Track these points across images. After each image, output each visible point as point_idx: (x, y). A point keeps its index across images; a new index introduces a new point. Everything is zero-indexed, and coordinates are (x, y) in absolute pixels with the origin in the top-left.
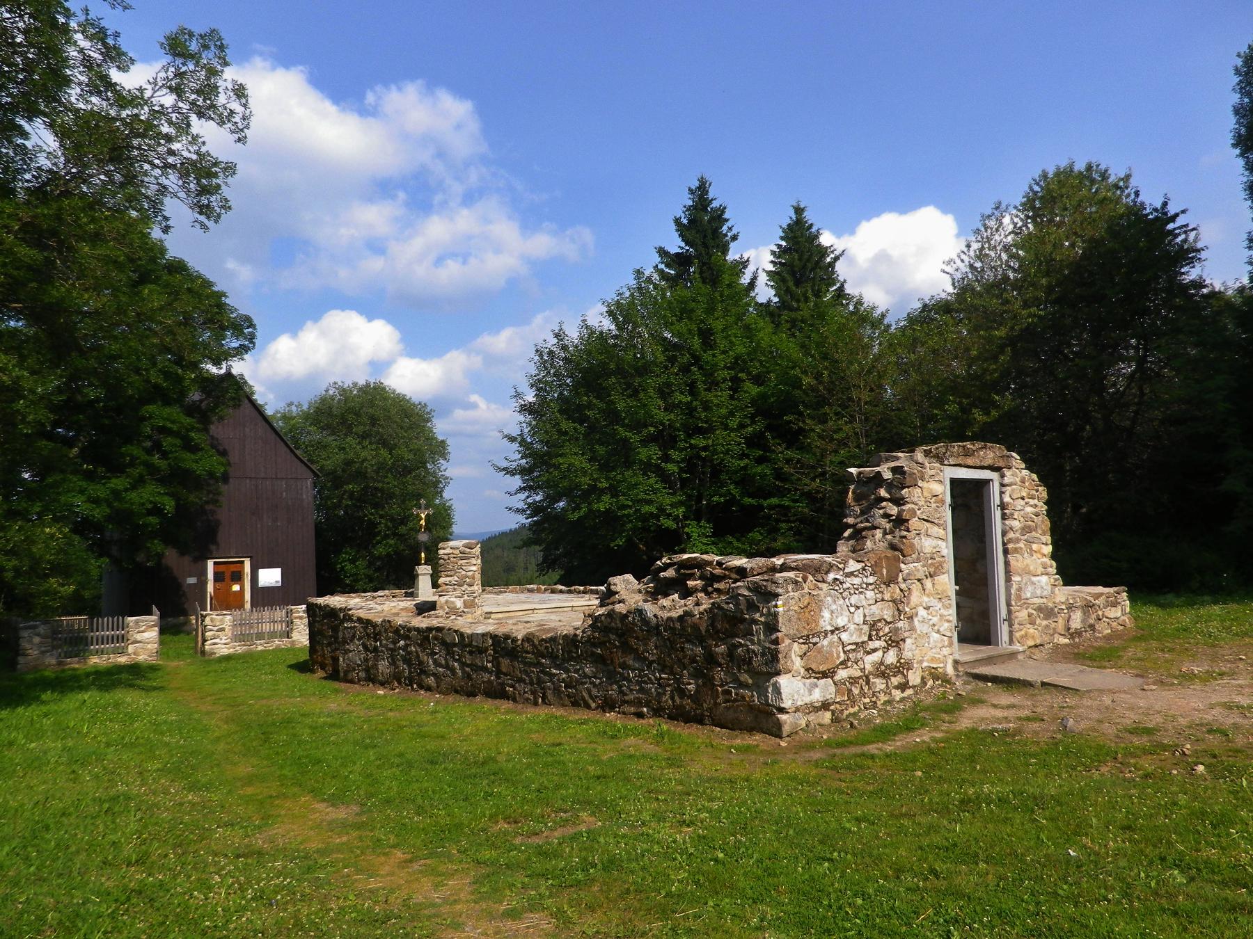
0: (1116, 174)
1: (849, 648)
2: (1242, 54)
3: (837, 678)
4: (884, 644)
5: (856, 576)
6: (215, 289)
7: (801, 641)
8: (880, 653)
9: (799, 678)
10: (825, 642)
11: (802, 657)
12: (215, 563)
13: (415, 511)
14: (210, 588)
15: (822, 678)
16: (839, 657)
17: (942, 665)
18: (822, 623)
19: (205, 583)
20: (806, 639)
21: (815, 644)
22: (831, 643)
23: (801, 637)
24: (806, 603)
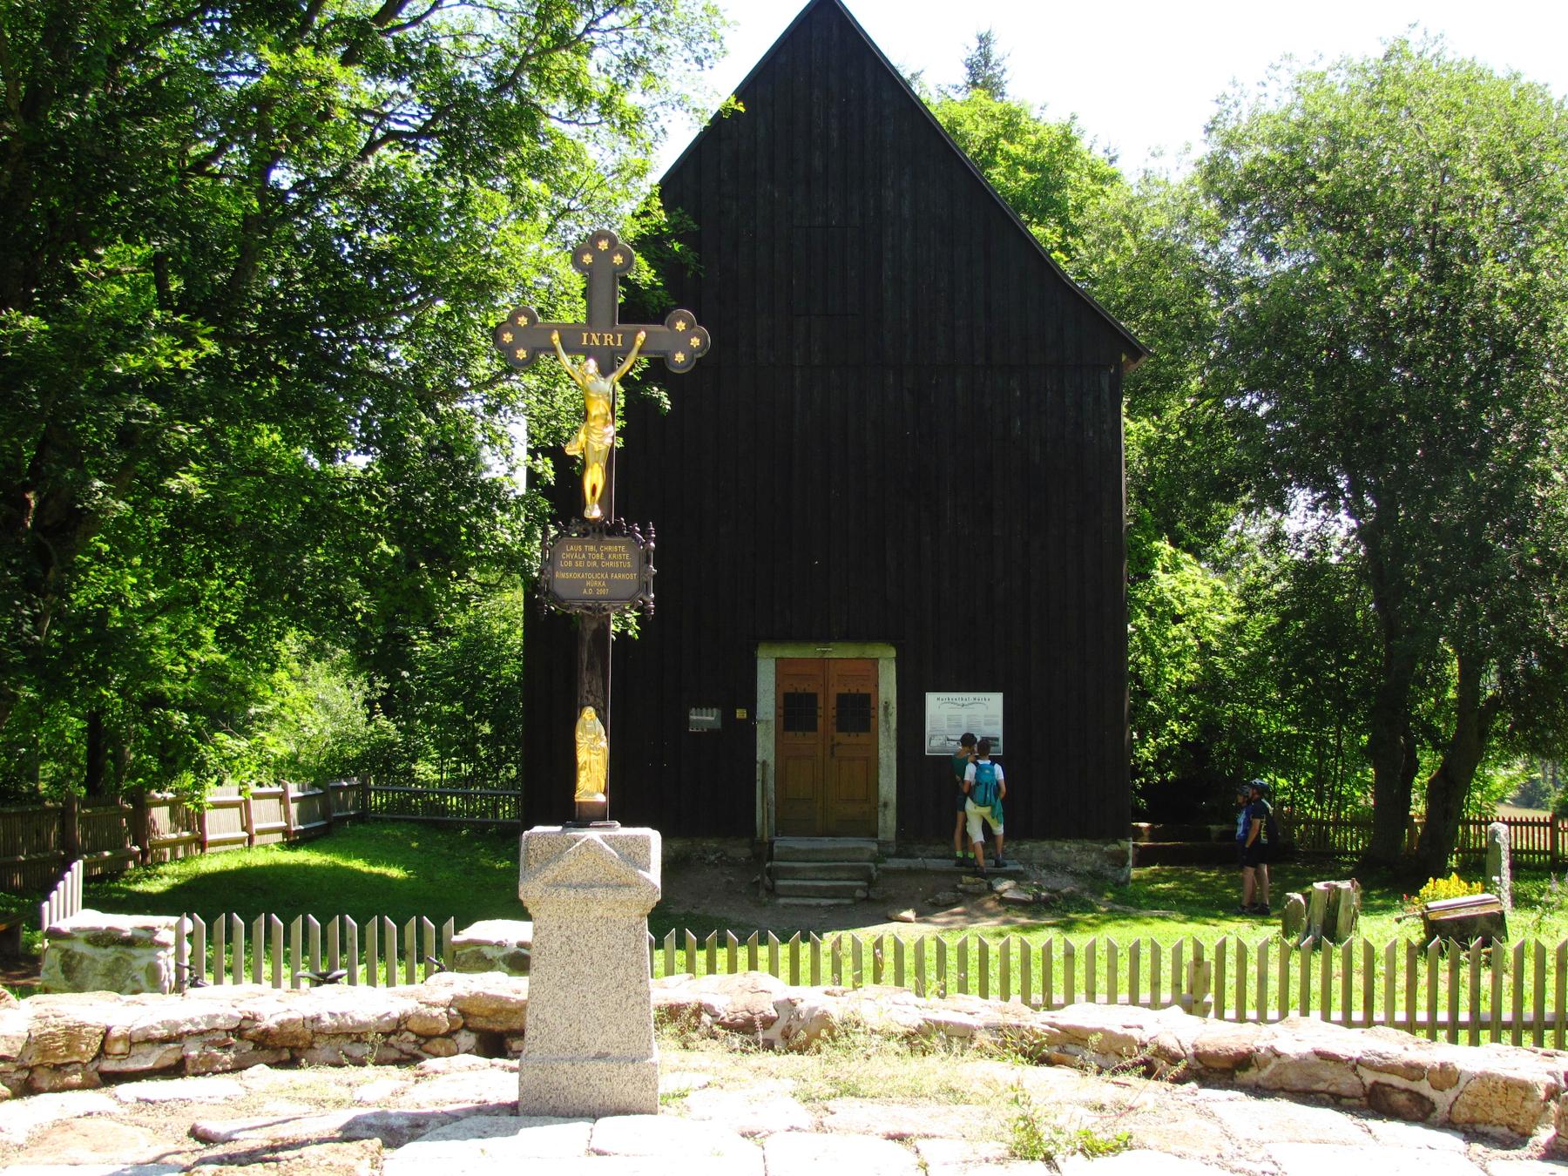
12: (780, 661)
14: (765, 747)
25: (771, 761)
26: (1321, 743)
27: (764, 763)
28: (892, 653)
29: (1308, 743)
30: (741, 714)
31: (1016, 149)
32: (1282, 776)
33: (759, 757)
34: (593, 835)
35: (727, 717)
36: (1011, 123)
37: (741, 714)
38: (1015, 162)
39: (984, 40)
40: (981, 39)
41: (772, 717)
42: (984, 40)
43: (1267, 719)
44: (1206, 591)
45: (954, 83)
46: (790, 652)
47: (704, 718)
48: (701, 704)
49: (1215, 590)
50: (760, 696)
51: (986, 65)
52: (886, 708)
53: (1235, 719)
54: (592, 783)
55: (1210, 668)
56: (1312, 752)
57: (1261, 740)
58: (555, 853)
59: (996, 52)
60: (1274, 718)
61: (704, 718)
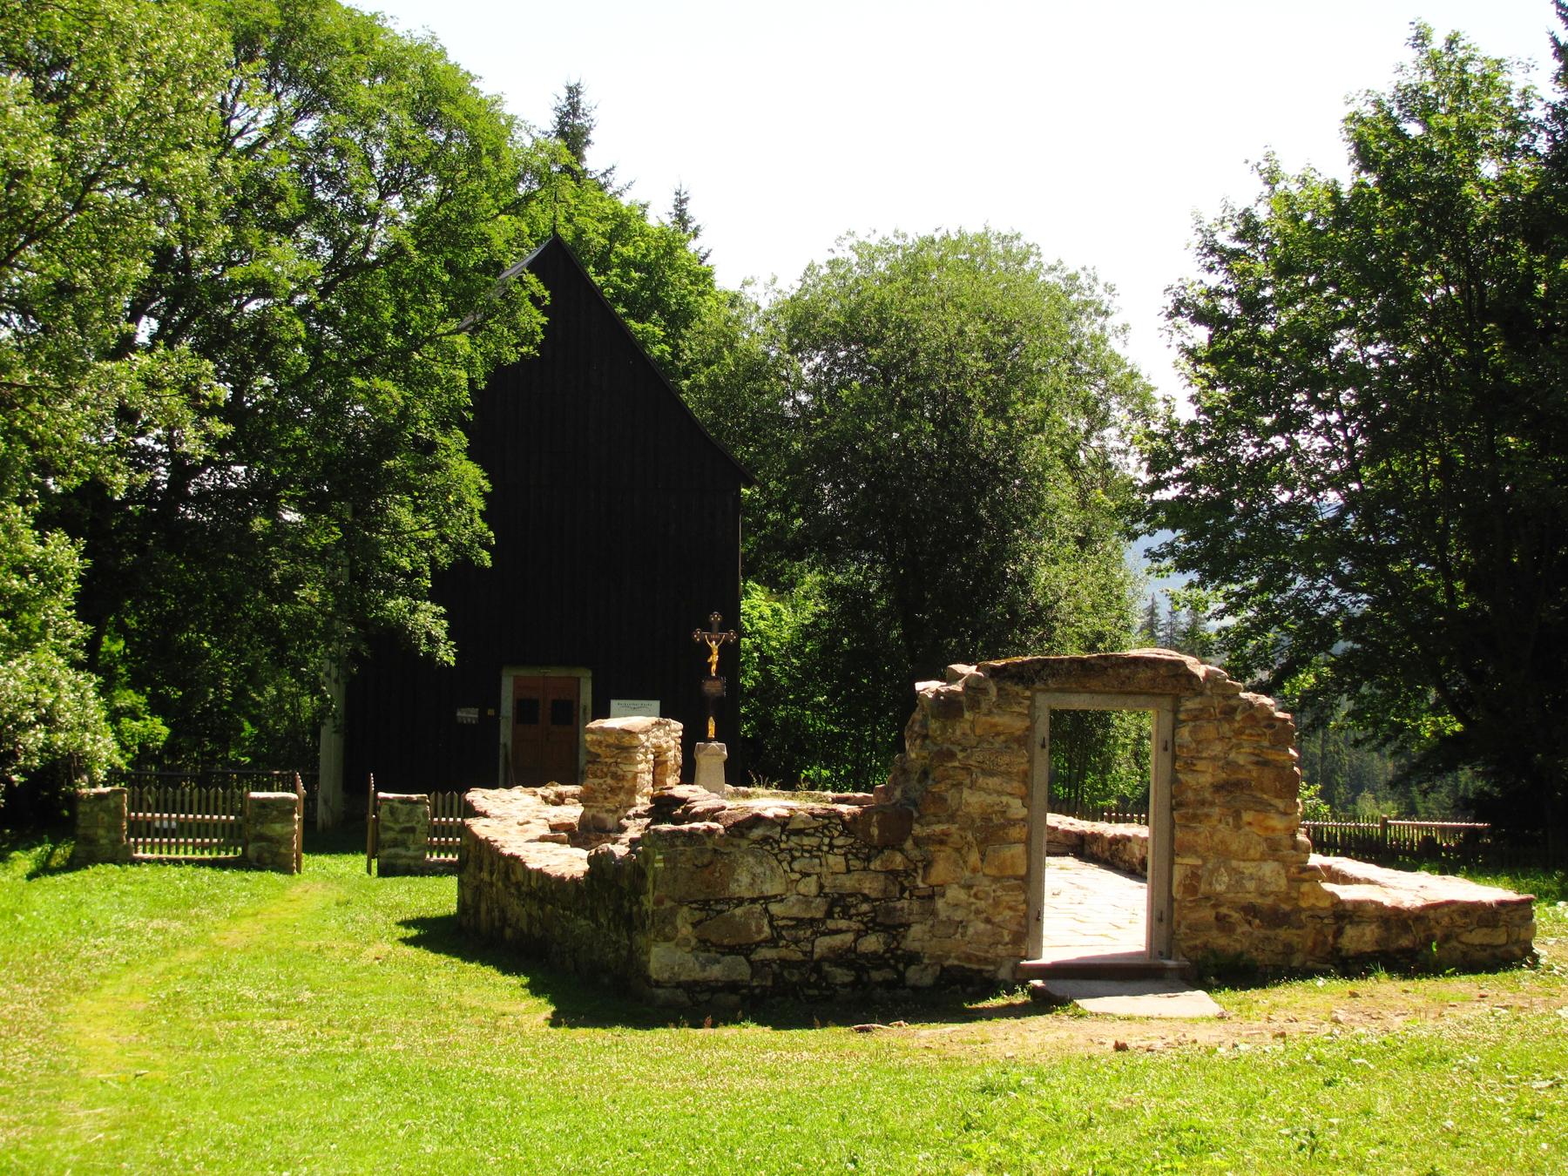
0: (1249, 195)
1: (781, 923)
2: (748, 290)
3: (754, 957)
4: (855, 926)
5: (808, 835)
6: (483, 96)
7: (694, 906)
8: (850, 937)
9: (688, 949)
10: (739, 911)
11: (694, 925)
12: (517, 679)
13: (698, 635)
14: (506, 734)
15: (729, 954)
16: (760, 931)
17: (991, 968)
18: (733, 887)
19: (495, 723)
20: (705, 905)
21: (721, 912)
22: (750, 913)
23: (695, 902)
24: (706, 861)
25: (509, 743)
26: (859, 740)
27: (505, 745)
28: (589, 674)
29: (847, 740)
30: (491, 712)
31: (628, 251)
32: (825, 768)
33: (502, 740)
34: (713, 744)
35: (482, 713)
36: (621, 224)
37: (491, 712)
38: (627, 264)
39: (573, 91)
40: (570, 89)
41: (510, 714)
42: (573, 91)
43: (813, 719)
44: (768, 613)
45: (545, 129)
46: (523, 672)
47: (468, 715)
48: (466, 704)
49: (776, 612)
50: (503, 698)
51: (574, 115)
52: (585, 709)
53: (785, 720)
54: (711, 733)
55: (767, 674)
56: (850, 747)
57: (810, 737)
58: (705, 748)
59: (585, 101)
60: (820, 719)
61: (468, 715)
